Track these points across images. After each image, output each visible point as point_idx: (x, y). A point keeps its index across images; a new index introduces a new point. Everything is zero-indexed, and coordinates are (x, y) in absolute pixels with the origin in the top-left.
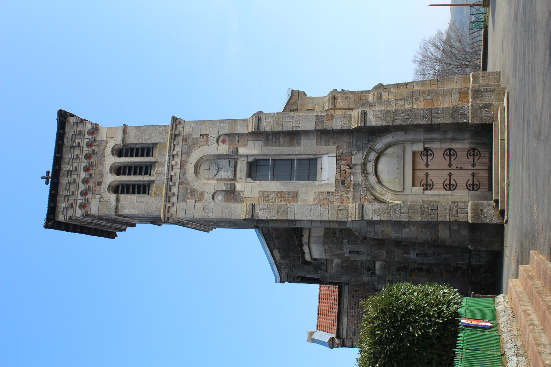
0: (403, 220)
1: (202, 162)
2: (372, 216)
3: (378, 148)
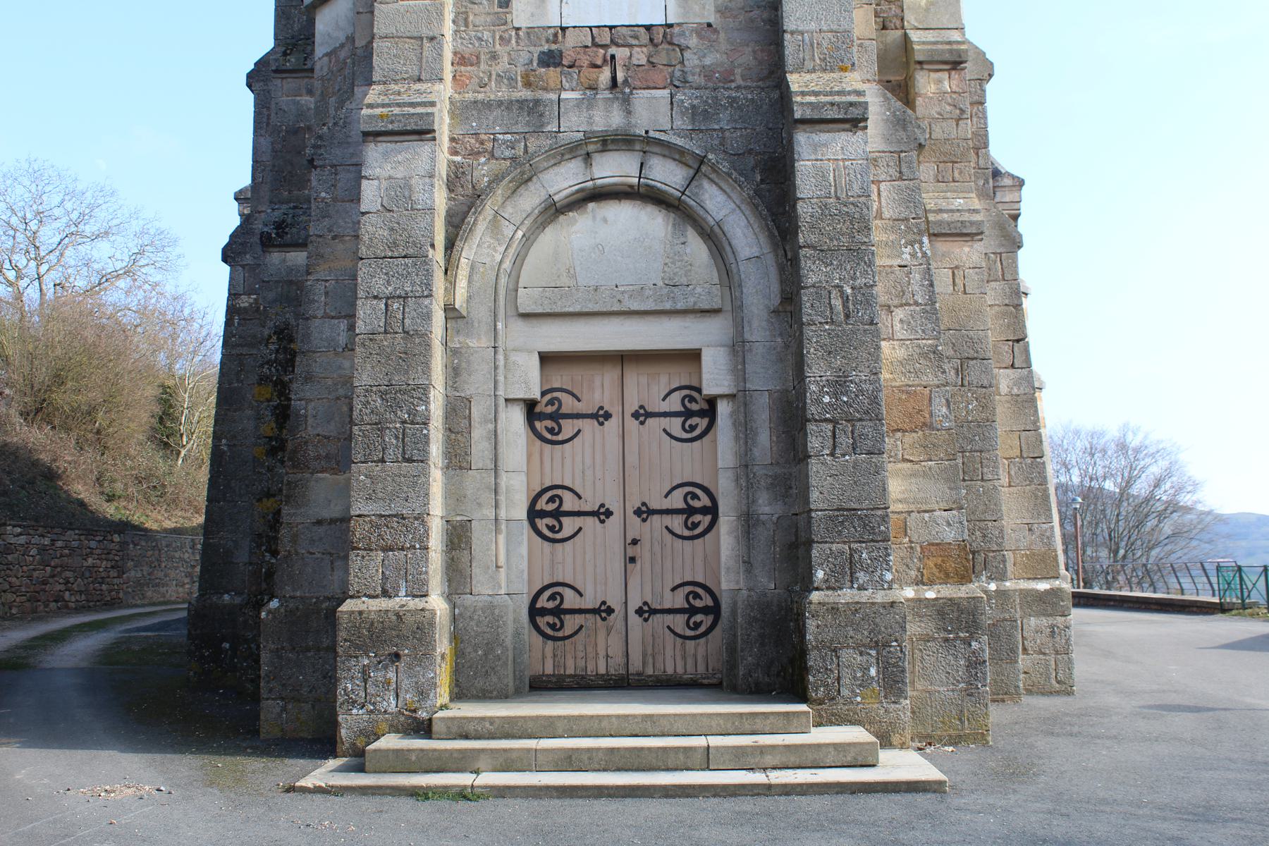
0: (360, 313)
2: (378, 178)
3: (707, 196)
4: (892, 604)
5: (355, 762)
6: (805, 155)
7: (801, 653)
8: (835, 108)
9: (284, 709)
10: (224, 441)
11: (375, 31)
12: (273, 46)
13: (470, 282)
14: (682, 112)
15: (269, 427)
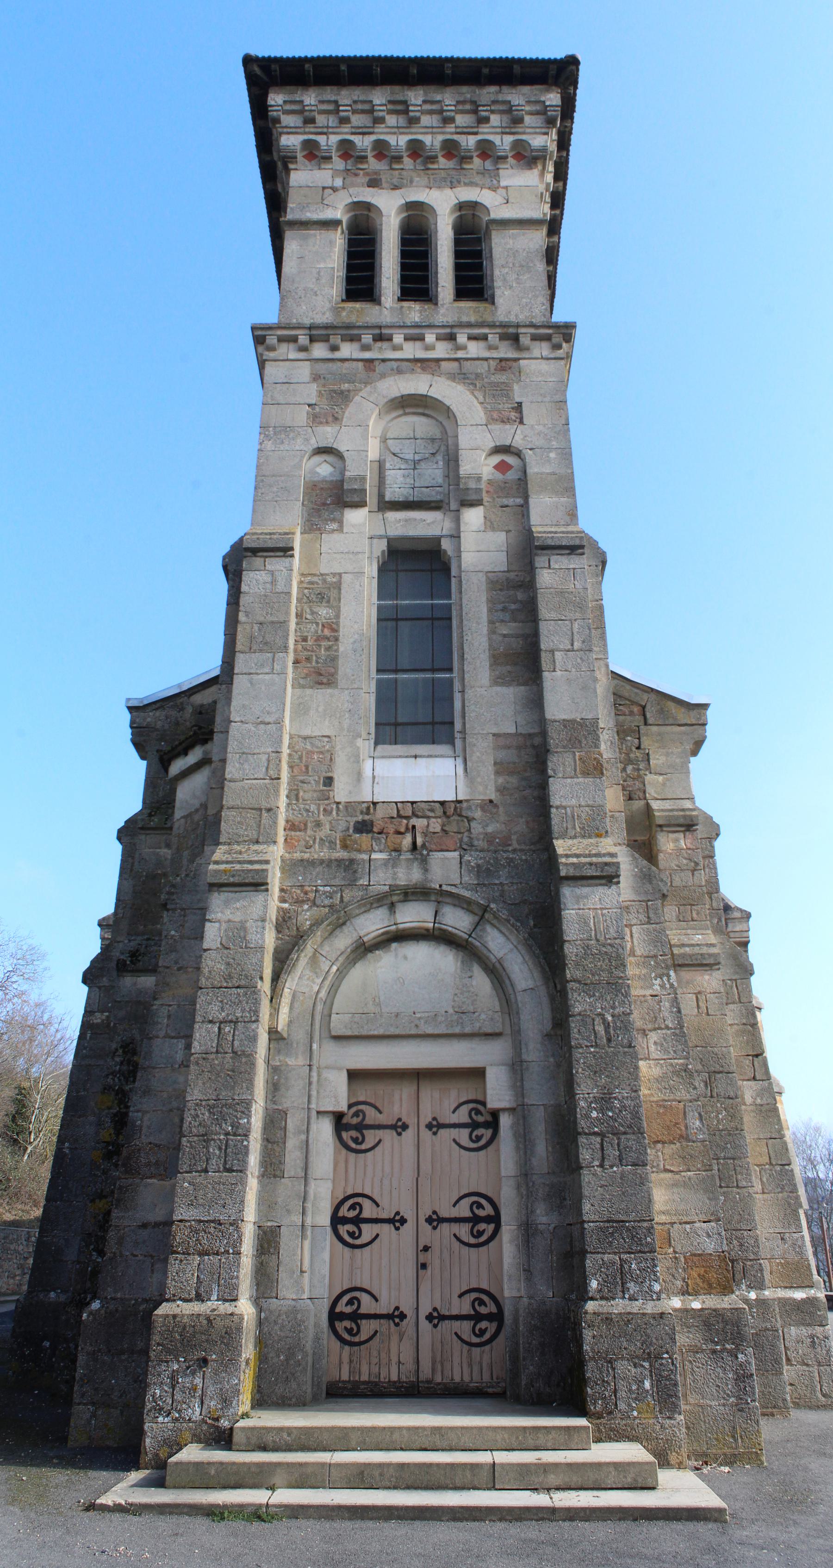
0: (197, 1035)
1: (437, 420)
2: (219, 921)
3: (489, 938)
4: (662, 1315)
5: (156, 1476)
6: (569, 905)
7: (578, 1363)
8: (593, 867)
9: (94, 1415)
10: (67, 1144)
11: (224, 803)
12: (140, 808)
13: (291, 1008)
14: (469, 870)
15: (107, 1134)
